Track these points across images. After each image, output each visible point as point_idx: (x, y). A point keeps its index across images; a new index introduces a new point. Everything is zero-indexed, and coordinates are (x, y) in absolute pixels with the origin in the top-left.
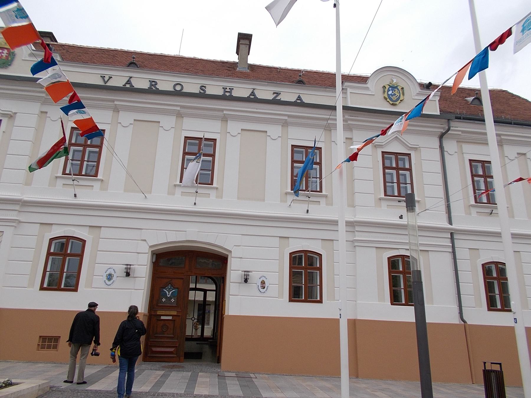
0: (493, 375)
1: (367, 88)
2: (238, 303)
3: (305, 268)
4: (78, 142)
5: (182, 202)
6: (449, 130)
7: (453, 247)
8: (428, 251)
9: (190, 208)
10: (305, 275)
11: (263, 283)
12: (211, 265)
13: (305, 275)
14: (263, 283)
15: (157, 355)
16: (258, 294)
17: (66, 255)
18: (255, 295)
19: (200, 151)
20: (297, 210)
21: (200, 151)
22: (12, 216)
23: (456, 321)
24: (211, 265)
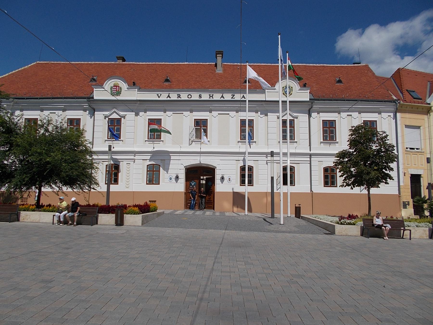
0: (298, 208)
1: (275, 89)
2: (220, 187)
3: (330, 174)
4: (111, 204)
5: (195, 148)
6: (312, 107)
7: (310, 161)
8: (299, 163)
9: (199, 150)
10: (246, 175)
11: (229, 179)
12: (210, 171)
13: (246, 175)
14: (229, 179)
15: (100, 157)
16: (228, 183)
17: (153, 171)
18: (227, 184)
19: (201, 126)
20: (244, 148)
21: (201, 126)
22: (132, 157)
23: (309, 191)
24: (210, 171)
